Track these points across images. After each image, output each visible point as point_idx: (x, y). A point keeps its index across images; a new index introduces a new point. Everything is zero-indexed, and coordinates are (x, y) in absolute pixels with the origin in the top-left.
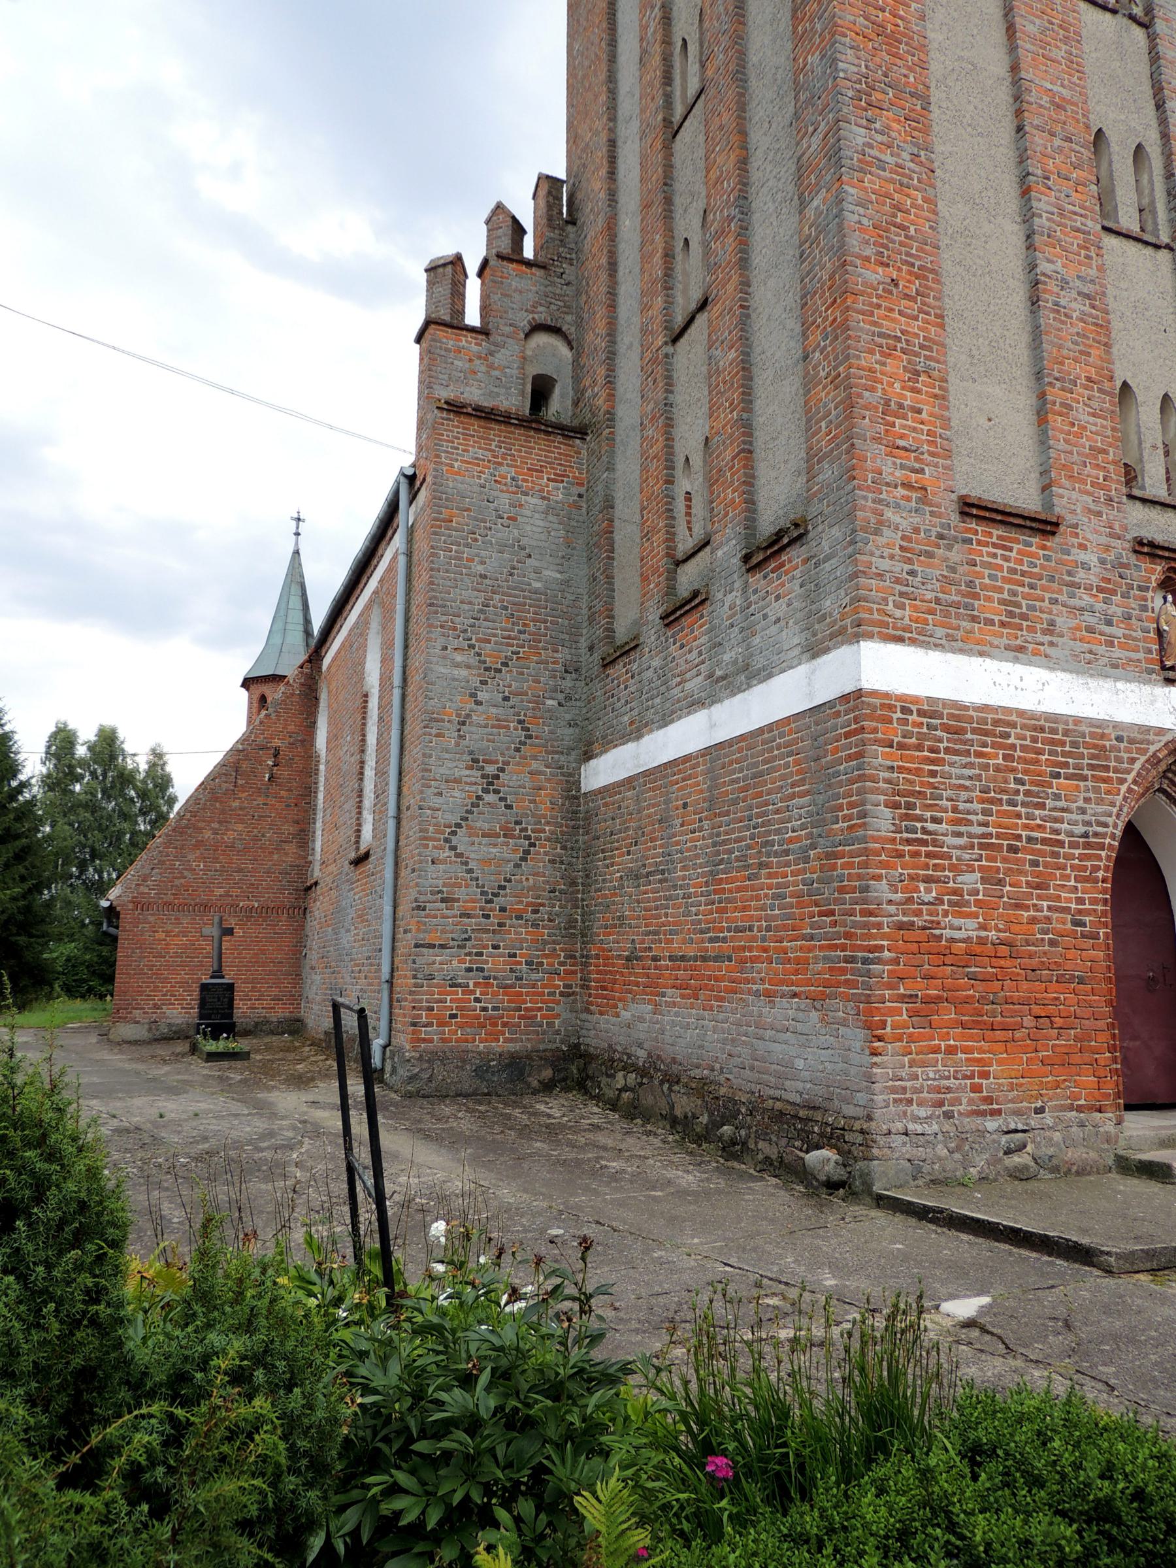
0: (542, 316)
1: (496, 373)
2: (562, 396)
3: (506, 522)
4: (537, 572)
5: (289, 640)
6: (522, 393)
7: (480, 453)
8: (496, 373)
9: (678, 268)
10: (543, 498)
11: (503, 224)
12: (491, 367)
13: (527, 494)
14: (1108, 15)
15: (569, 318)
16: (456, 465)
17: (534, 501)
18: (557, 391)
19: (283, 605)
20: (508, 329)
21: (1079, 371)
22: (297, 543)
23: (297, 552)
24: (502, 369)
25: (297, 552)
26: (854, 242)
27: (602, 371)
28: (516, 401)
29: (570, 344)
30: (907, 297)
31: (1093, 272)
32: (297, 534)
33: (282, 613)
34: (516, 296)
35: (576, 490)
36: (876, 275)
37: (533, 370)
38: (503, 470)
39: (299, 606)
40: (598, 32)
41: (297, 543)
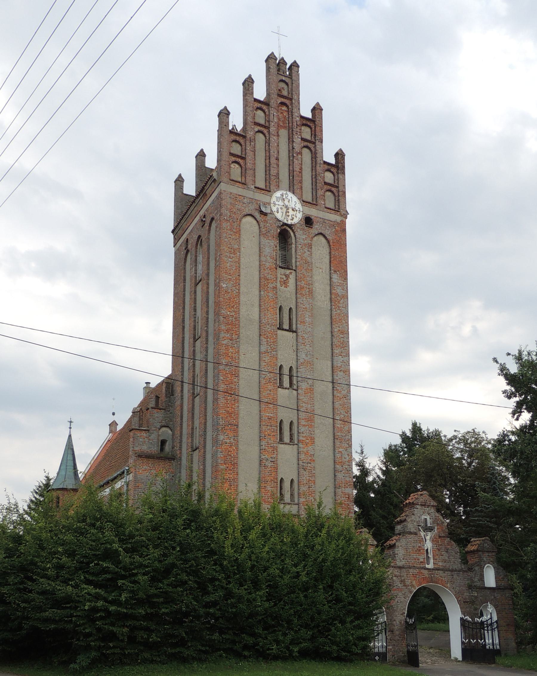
0: (164, 423)
1: (151, 441)
2: (169, 445)
5: (68, 473)
6: (158, 446)
7: (146, 467)
8: (151, 441)
9: (195, 433)
12: (149, 440)
14: (287, 390)
15: (171, 423)
18: (167, 444)
19: (65, 458)
20: (154, 429)
21: (269, 479)
22: (70, 432)
23: (70, 436)
24: (152, 440)
25: (70, 436)
26: (219, 461)
27: (178, 445)
28: (155, 449)
29: (171, 430)
30: (230, 470)
31: (275, 456)
32: (70, 428)
33: (65, 461)
34: (157, 419)
35: (172, 475)
36: (223, 467)
37: (161, 438)
38: (152, 471)
39: (72, 459)
40: (180, 345)
41: (70, 432)
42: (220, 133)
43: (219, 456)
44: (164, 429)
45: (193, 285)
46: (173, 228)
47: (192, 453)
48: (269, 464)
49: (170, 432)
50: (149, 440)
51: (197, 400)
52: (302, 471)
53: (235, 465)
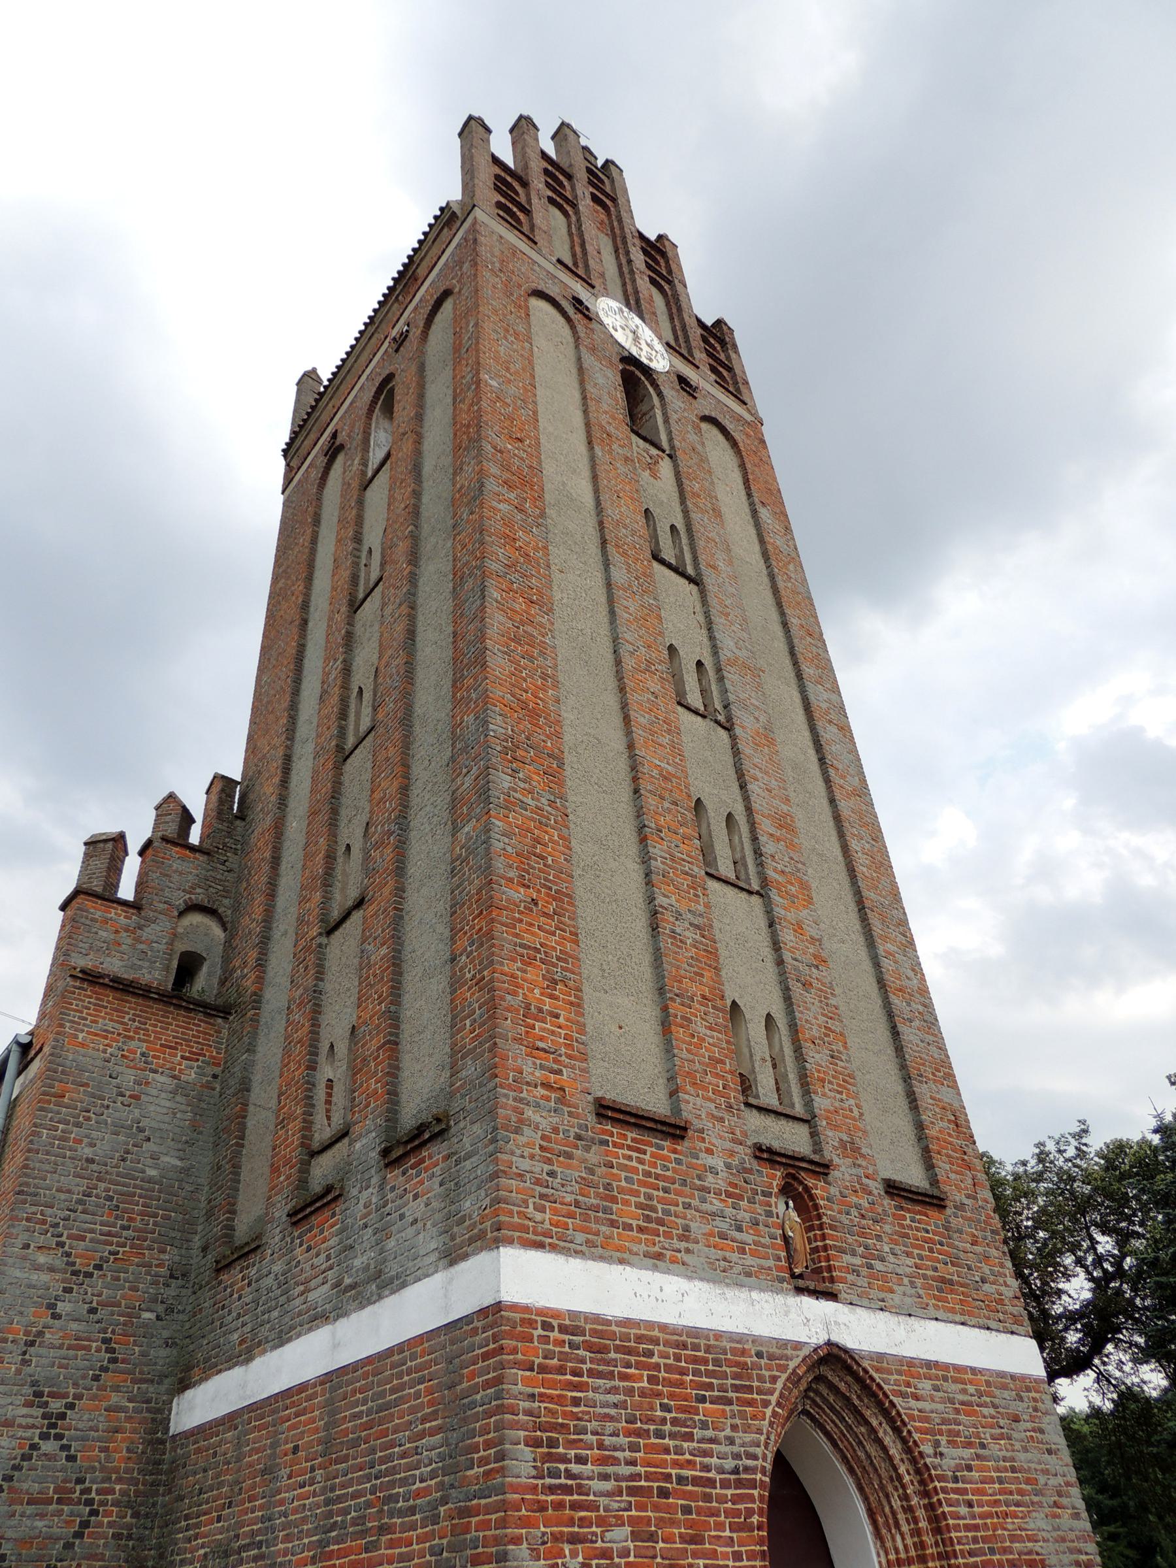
0: (200, 897)
2: (209, 974)
3: (127, 1100)
4: (154, 1157)
10: (174, 1077)
11: (173, 812)
12: (138, 940)
13: (155, 1072)
15: (226, 902)
16: (81, 1036)
17: (162, 1079)
21: (694, 989)
26: (499, 864)
30: (545, 915)
31: (701, 908)
34: (176, 877)
35: (210, 1070)
36: (518, 894)
37: (181, 947)
38: (133, 1044)
42: (468, 166)
43: (497, 846)
44: (196, 919)
45: (355, 484)
46: (287, 440)
47: (324, 940)
48: (690, 936)
49: (217, 932)
50: (138, 940)
51: (359, 766)
52: (796, 989)
53: (563, 898)
